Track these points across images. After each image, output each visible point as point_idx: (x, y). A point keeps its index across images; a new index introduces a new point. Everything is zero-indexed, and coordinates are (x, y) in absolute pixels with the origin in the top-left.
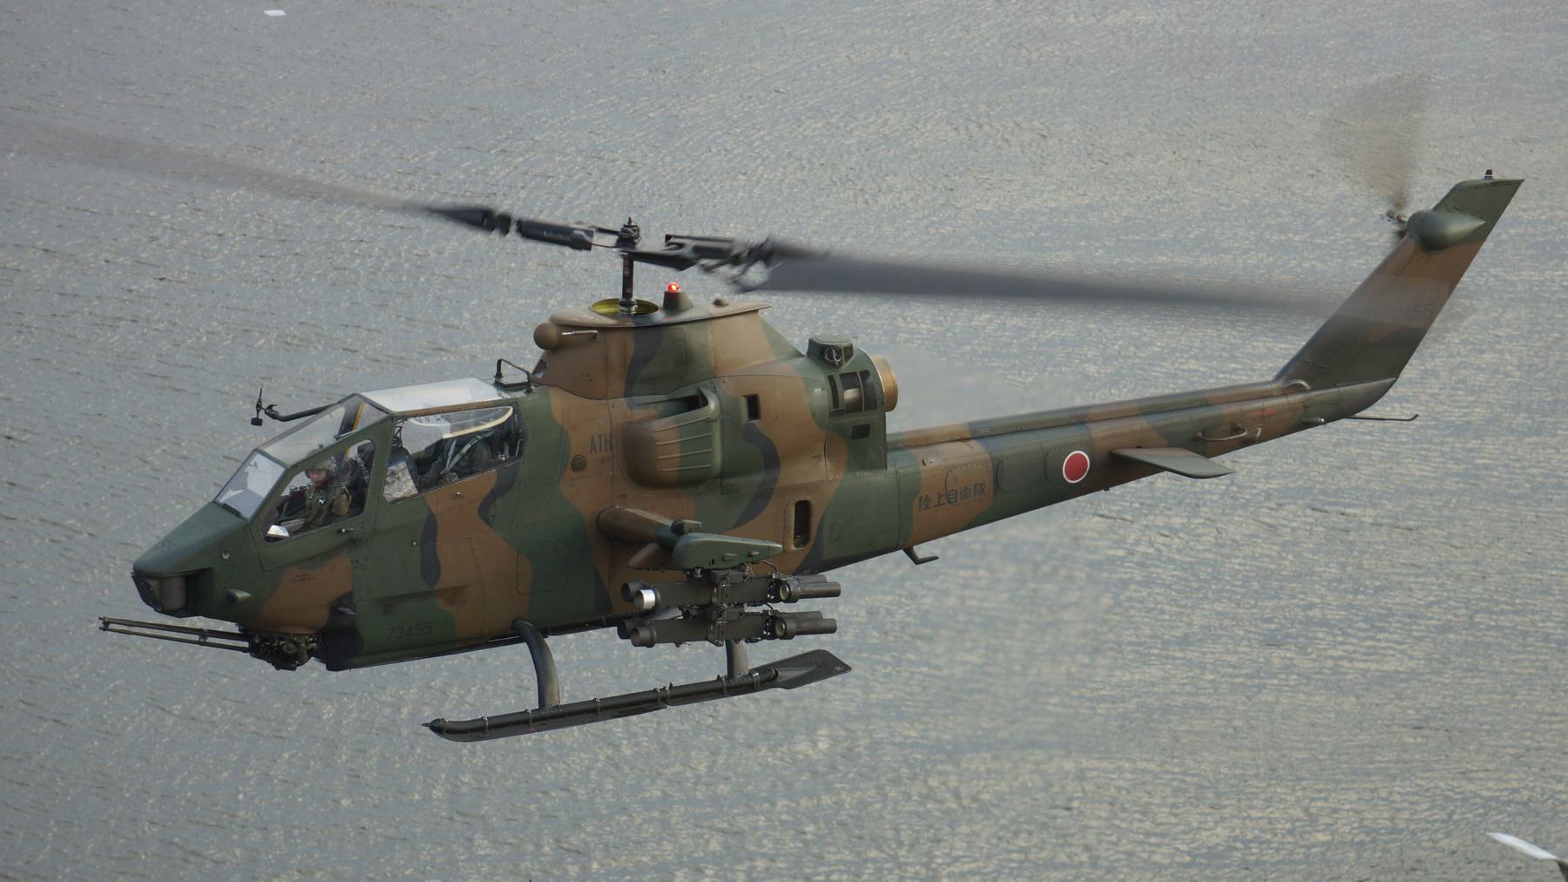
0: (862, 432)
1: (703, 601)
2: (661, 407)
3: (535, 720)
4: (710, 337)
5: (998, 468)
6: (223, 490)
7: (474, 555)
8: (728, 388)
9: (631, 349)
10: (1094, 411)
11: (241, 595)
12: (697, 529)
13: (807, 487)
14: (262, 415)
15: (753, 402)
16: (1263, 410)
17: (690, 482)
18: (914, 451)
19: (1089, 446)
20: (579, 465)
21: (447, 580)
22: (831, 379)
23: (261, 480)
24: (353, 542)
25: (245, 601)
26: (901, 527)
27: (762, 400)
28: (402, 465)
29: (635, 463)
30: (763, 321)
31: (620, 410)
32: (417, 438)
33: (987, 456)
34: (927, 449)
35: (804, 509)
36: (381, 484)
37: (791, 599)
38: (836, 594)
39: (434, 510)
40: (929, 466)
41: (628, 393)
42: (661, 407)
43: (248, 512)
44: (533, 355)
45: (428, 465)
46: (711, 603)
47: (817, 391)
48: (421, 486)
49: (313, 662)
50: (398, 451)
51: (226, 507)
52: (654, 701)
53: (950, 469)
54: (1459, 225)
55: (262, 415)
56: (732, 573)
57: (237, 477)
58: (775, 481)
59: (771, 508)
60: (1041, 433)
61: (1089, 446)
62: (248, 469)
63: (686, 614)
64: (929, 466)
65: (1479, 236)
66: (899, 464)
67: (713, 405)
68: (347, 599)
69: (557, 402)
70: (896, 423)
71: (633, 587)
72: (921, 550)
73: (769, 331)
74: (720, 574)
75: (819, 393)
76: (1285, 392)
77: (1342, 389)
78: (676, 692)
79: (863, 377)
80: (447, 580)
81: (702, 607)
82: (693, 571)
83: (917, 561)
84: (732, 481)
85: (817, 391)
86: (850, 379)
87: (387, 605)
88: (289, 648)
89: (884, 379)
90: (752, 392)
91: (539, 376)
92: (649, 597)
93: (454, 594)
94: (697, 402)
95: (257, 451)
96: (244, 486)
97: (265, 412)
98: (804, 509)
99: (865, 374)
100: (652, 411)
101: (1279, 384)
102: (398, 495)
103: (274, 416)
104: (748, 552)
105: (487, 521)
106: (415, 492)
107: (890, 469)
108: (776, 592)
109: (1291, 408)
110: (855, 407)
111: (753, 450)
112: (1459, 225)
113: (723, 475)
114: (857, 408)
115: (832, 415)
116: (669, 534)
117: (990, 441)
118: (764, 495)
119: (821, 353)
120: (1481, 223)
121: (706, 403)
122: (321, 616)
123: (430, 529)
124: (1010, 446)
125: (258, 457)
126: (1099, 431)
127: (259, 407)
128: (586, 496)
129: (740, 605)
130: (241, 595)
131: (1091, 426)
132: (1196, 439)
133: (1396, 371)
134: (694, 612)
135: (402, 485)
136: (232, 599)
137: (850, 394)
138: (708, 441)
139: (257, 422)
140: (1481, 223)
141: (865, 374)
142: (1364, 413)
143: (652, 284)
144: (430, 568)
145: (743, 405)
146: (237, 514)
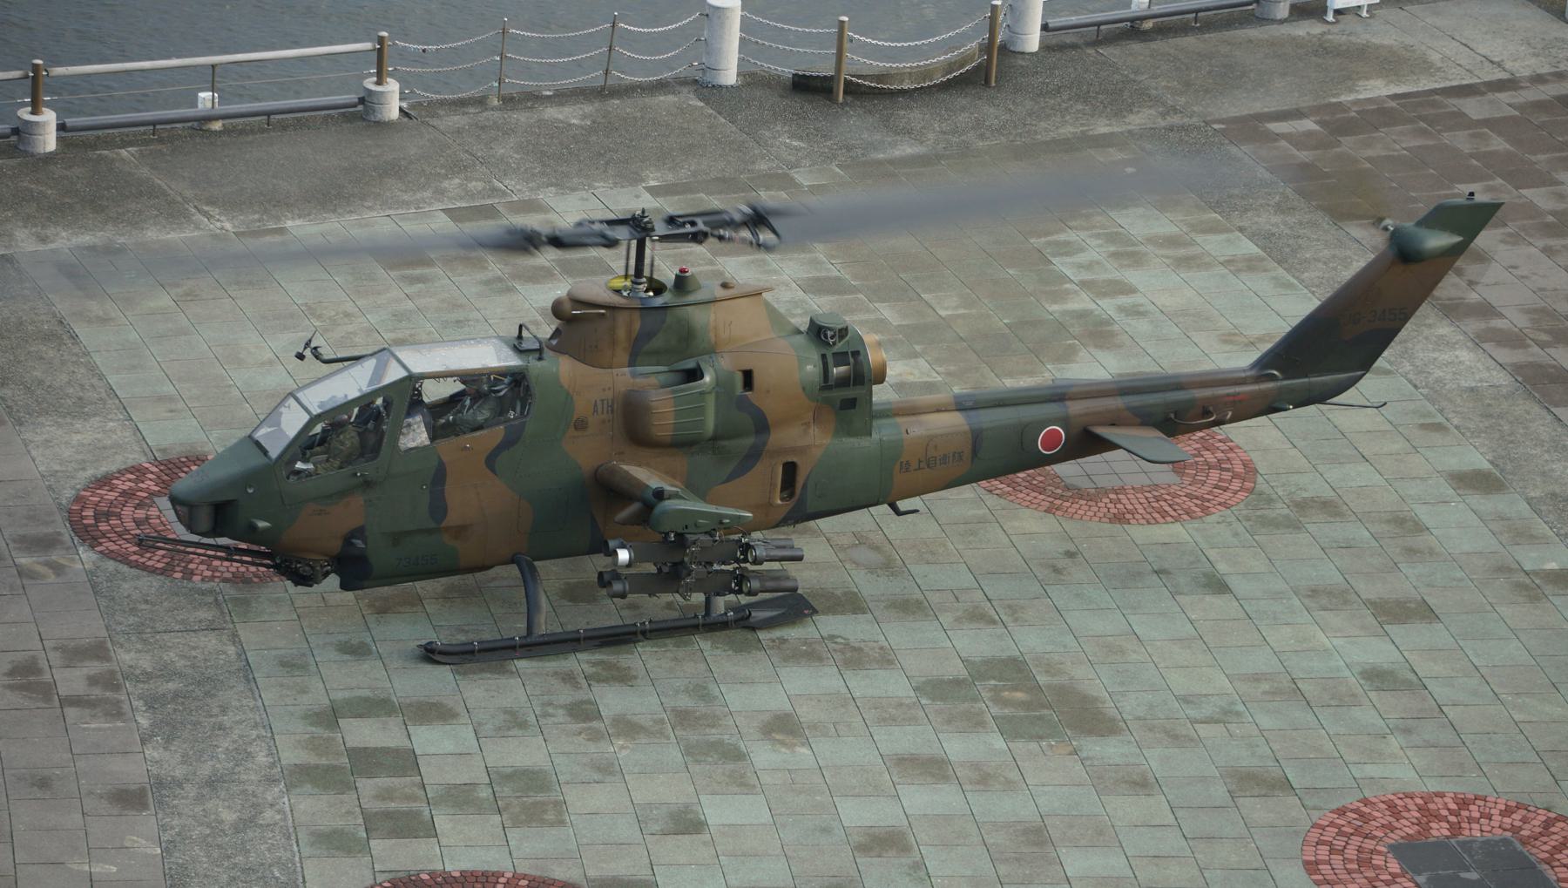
0: (850, 404)
1: (677, 560)
2: (662, 377)
3: (522, 646)
4: (712, 317)
5: (977, 437)
6: (256, 429)
7: (477, 498)
8: (726, 363)
9: (637, 326)
10: (1074, 390)
11: (262, 524)
12: (676, 496)
13: (794, 450)
14: (308, 353)
15: (748, 376)
16: (1234, 395)
17: (683, 444)
18: (899, 420)
19: (1065, 422)
20: (581, 425)
21: (453, 519)
22: (824, 357)
23: (293, 422)
24: (367, 484)
25: (266, 530)
26: (884, 485)
27: (756, 375)
28: (419, 418)
29: (632, 424)
30: (767, 304)
31: (622, 378)
32: (434, 392)
33: (967, 428)
34: (913, 418)
35: (790, 470)
36: (397, 432)
37: (756, 561)
38: (800, 559)
39: (445, 459)
40: (912, 434)
41: (632, 364)
42: (662, 377)
43: (274, 453)
44: (546, 329)
45: (446, 417)
46: (682, 562)
47: (809, 368)
48: (433, 438)
49: (426, 400)
50: (416, 403)
51: (258, 444)
52: (635, 633)
53: (931, 438)
54: (1437, 241)
55: (308, 353)
56: (703, 537)
57: (272, 416)
58: (765, 444)
59: (760, 468)
60: (1021, 408)
61: (1065, 422)
62: (283, 409)
63: (660, 570)
64: (912, 434)
65: (1456, 252)
66: (883, 432)
67: (707, 379)
68: (359, 532)
69: (564, 368)
70: (881, 394)
71: (612, 544)
72: (903, 505)
73: (771, 311)
74: (693, 537)
75: (812, 369)
76: (1258, 379)
77: (1314, 379)
78: (654, 626)
79: (855, 355)
80: (453, 519)
81: (675, 564)
82: (667, 534)
83: (898, 513)
84: (726, 443)
85: (809, 368)
86: (841, 358)
87: (397, 538)
88: (304, 569)
89: (873, 357)
90: (747, 367)
91: (554, 342)
92: (623, 555)
93: (460, 531)
94: (694, 375)
95: (292, 394)
96: (278, 424)
97: (309, 352)
98: (790, 470)
99: (856, 354)
100: (653, 380)
101: (1253, 373)
102: (412, 445)
103: (317, 356)
104: (719, 519)
105: (493, 471)
106: (428, 442)
107: (874, 435)
108: (744, 553)
109: (1263, 394)
110: (843, 382)
111: (738, 432)
112: (1437, 241)
113: (715, 438)
114: (846, 380)
115: (823, 389)
116: (649, 495)
117: (973, 413)
118: (753, 456)
119: (817, 332)
120: (1457, 239)
121: (702, 377)
122: (336, 546)
123: (440, 475)
124: (990, 418)
125: (291, 401)
126: (1075, 408)
127: (307, 345)
128: (586, 453)
129: (711, 564)
130: (262, 524)
131: (1068, 403)
132: (1168, 419)
133: (1366, 365)
134: (665, 569)
135: (416, 435)
136: (254, 528)
137: (837, 371)
138: (701, 410)
139: (300, 357)
140: (1457, 239)
141: (856, 354)
142: (1335, 400)
143: (665, 262)
144: (438, 507)
145: (739, 378)
146: (265, 452)
